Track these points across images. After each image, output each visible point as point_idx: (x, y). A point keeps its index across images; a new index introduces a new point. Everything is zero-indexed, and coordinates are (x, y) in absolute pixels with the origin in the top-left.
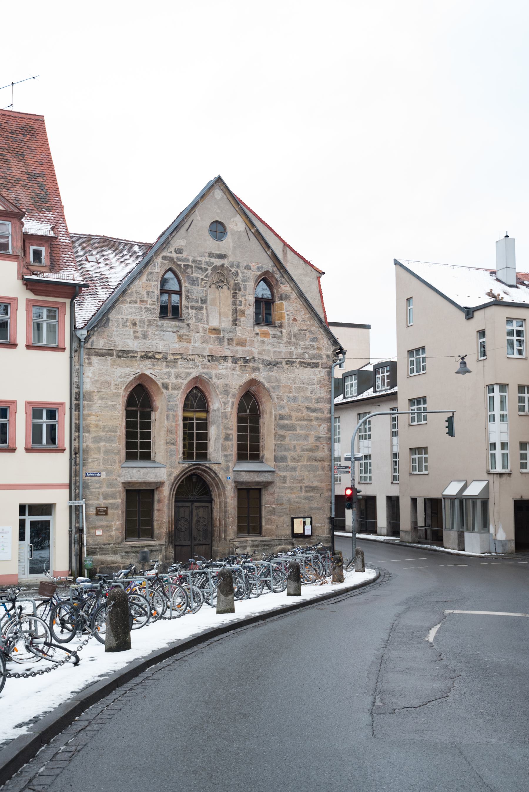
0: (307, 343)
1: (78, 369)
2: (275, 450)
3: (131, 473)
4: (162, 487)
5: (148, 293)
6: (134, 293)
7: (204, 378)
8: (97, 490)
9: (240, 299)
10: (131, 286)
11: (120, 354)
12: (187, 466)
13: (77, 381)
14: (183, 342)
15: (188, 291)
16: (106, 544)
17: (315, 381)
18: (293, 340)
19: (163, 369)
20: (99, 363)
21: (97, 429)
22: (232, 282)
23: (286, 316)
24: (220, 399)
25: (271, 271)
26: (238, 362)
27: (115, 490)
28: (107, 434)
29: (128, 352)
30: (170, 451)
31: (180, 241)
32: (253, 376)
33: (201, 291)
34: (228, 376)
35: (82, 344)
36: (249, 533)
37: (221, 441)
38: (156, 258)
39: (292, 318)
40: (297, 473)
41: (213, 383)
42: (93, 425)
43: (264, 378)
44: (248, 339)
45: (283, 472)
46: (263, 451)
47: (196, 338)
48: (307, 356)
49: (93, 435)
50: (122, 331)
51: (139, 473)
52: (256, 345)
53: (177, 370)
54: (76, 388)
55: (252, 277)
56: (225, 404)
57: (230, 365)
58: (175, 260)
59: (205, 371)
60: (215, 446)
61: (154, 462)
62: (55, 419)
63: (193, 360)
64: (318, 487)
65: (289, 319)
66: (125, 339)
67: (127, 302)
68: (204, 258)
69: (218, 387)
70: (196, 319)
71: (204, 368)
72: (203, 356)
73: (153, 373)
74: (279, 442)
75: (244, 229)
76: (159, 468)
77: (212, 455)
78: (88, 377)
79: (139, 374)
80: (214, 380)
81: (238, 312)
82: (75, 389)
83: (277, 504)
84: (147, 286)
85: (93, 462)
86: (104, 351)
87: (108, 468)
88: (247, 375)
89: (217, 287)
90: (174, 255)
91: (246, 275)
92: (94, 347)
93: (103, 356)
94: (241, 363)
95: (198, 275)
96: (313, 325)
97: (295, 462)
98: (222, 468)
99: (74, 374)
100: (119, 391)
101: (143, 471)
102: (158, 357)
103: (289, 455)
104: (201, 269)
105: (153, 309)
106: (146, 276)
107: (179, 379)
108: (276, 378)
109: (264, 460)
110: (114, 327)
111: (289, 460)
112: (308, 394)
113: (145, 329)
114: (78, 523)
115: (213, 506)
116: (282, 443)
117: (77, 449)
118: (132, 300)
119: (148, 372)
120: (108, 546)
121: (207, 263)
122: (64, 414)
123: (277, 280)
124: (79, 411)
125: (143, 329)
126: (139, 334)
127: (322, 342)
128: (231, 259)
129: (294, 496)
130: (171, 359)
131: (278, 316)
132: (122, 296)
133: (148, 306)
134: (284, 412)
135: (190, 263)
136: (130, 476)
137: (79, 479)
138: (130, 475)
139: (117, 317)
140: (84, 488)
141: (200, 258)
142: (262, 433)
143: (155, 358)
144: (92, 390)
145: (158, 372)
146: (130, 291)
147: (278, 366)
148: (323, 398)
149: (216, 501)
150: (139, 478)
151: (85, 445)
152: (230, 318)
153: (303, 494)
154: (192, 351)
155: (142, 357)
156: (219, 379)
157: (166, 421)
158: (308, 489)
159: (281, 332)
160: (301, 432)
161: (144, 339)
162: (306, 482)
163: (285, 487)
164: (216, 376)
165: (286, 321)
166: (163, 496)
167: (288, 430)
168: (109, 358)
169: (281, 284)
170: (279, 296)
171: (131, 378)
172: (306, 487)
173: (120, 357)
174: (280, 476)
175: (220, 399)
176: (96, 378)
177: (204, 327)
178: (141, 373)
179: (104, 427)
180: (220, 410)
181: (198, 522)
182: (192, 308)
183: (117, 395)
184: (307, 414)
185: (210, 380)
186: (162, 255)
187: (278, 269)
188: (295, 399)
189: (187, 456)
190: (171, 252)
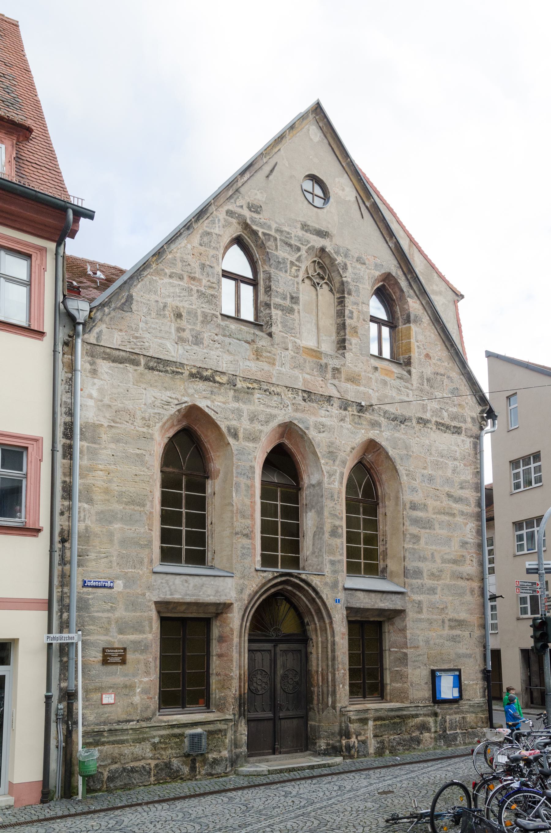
3: (171, 583)
4: (226, 613)
6: (178, 260)
7: (298, 429)
8: (106, 615)
9: (350, 308)
11: (151, 364)
12: (270, 576)
16: (122, 722)
17: (458, 454)
18: (426, 387)
21: (107, 497)
24: (323, 466)
25: (394, 274)
27: (141, 616)
28: (127, 507)
29: (167, 363)
30: (242, 548)
31: (256, 191)
32: (373, 434)
33: (291, 282)
34: (334, 428)
39: (425, 352)
40: (437, 596)
41: (310, 437)
42: (100, 488)
43: (387, 439)
45: (418, 594)
46: (384, 561)
48: (445, 414)
49: (99, 507)
50: (157, 323)
51: (186, 585)
53: (252, 408)
55: (367, 278)
58: (249, 221)
59: (298, 415)
60: (313, 545)
61: (212, 567)
65: (420, 354)
67: (166, 274)
68: (294, 230)
71: (296, 410)
73: (212, 407)
74: (411, 546)
75: (354, 199)
76: (222, 578)
77: (309, 562)
79: (186, 404)
80: (312, 434)
85: (96, 560)
86: (122, 353)
87: (127, 573)
88: (363, 431)
90: (247, 213)
91: (358, 272)
94: (353, 410)
95: (286, 255)
98: (326, 584)
102: (221, 381)
104: (290, 245)
105: (212, 295)
106: (199, 236)
107: (257, 423)
108: (404, 442)
109: (388, 575)
111: (425, 575)
112: (449, 473)
113: (198, 327)
114: (66, 679)
117: (66, 532)
118: (173, 273)
119: (202, 404)
122: (41, 460)
124: (71, 459)
126: (187, 335)
129: (434, 634)
131: (404, 348)
132: (156, 260)
133: (202, 289)
135: (272, 233)
136: (170, 590)
138: (169, 587)
139: (147, 296)
140: (79, 609)
142: (381, 532)
143: (215, 382)
145: (220, 407)
146: (170, 256)
147: (406, 424)
148: (469, 483)
149: (314, 640)
150: (187, 594)
151: (82, 526)
155: (192, 375)
156: (320, 432)
158: (453, 624)
159: (409, 372)
161: (196, 344)
162: (449, 613)
163: (420, 620)
164: (316, 426)
166: (228, 628)
167: (423, 528)
168: (130, 368)
170: (405, 316)
171: (173, 410)
172: (449, 620)
173: (152, 369)
176: (106, 401)
178: (190, 404)
179: (121, 494)
184: (448, 504)
185: (307, 431)
186: (226, 208)
187: (405, 274)
188: (431, 479)
190: (242, 207)
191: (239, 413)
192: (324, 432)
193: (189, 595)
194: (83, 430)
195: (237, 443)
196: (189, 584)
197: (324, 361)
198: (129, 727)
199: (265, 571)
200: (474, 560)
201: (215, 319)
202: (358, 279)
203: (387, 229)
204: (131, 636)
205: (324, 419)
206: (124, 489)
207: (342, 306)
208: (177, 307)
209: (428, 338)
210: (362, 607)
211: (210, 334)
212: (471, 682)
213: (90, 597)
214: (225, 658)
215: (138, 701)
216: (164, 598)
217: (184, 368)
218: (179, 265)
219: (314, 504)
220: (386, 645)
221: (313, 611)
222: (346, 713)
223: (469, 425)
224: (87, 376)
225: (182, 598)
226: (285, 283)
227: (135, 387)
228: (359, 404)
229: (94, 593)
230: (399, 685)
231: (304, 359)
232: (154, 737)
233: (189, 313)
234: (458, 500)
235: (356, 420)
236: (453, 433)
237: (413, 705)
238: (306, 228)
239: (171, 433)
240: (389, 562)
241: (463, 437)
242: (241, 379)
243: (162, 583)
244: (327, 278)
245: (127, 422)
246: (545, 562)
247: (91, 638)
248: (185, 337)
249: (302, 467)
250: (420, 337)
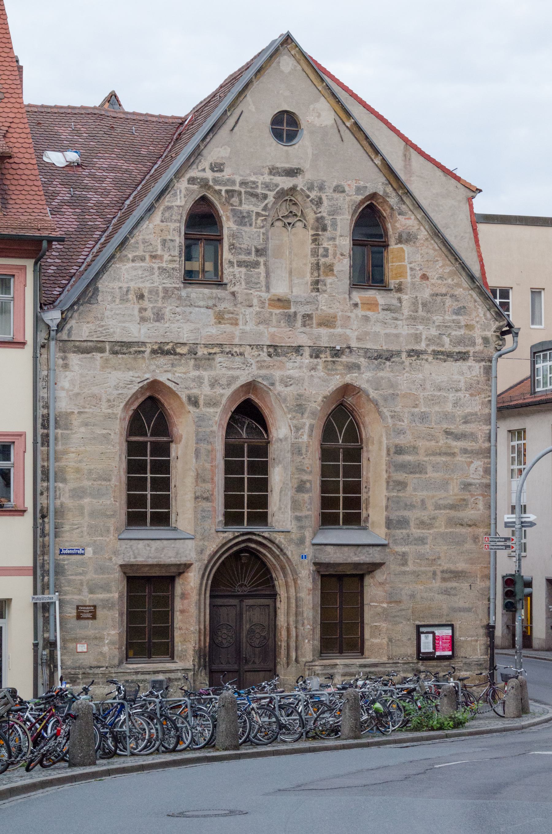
0: (447, 317)
1: (47, 376)
2: (387, 507)
3: (134, 548)
4: (188, 572)
5: (164, 242)
6: (140, 243)
7: (262, 386)
9: (325, 245)
10: (135, 232)
11: (117, 348)
12: (231, 536)
13: (46, 395)
14: (225, 324)
16: (94, 668)
18: (421, 313)
19: (189, 372)
20: (80, 365)
21: (79, 476)
22: (311, 217)
23: (408, 271)
26: (321, 356)
28: (95, 483)
31: (219, 149)
32: (349, 378)
34: (303, 380)
36: (341, 652)
38: (178, 181)
39: (420, 274)
40: (427, 546)
42: (72, 468)
43: (368, 381)
44: (340, 314)
45: (402, 545)
46: (367, 510)
47: (248, 317)
49: (71, 485)
50: (120, 308)
51: (148, 548)
52: (355, 324)
53: (213, 373)
54: (43, 407)
57: (307, 361)
58: (211, 183)
59: (263, 372)
60: (280, 501)
62: (10, 461)
63: (242, 354)
64: (466, 572)
65: (413, 276)
66: (124, 322)
67: (129, 259)
72: (259, 347)
73: (173, 380)
74: (395, 494)
75: (333, 122)
76: (182, 541)
78: (63, 389)
79: (148, 381)
81: (322, 268)
82: (42, 409)
84: (162, 231)
86: (89, 344)
87: (95, 541)
88: (338, 377)
90: (209, 175)
92: (73, 338)
93: (88, 353)
94: (326, 357)
96: (458, 285)
97: (424, 529)
99: (40, 384)
100: (115, 412)
102: (181, 352)
103: (412, 515)
107: (218, 387)
108: (389, 381)
110: (106, 303)
112: (449, 407)
113: (160, 304)
116: (401, 494)
117: (45, 509)
119: (163, 378)
120: (97, 671)
121: (267, 186)
125: (155, 305)
128: (309, 176)
129: (422, 587)
130: (204, 354)
133: (164, 265)
135: (237, 188)
136: (134, 554)
137: (49, 560)
138: (133, 552)
139: (111, 285)
140: (57, 573)
141: (254, 177)
143: (175, 354)
144: (69, 411)
147: (393, 360)
148: (477, 415)
150: (148, 557)
151: (58, 502)
152: (309, 278)
153: (438, 585)
154: (240, 339)
155: (154, 352)
156: (286, 386)
157: (194, 460)
158: (446, 576)
159: (400, 300)
160: (435, 475)
161: (158, 321)
162: (443, 564)
163: (404, 573)
164: (282, 381)
168: (98, 355)
169: (399, 214)
170: (397, 235)
171: (135, 388)
172: (443, 572)
173: (115, 353)
174: (396, 552)
175: (289, 421)
176: (76, 390)
177: (260, 297)
178: (151, 379)
179: (90, 472)
180: (289, 440)
181: (251, 631)
185: (272, 388)
186: (188, 176)
187: (394, 189)
188: (424, 417)
190: (204, 170)
192: (291, 385)
193: (151, 557)
194: (58, 419)
195: (197, 411)
196: (151, 548)
198: (99, 672)
199: (226, 532)
203: (372, 147)
204: (100, 595)
205: (291, 371)
206: (92, 467)
207: (316, 245)
208: (139, 288)
209: (426, 256)
210: (332, 562)
211: (171, 308)
212: (469, 639)
213: (65, 563)
214: (187, 614)
215: (107, 651)
216: (128, 561)
217: (145, 346)
218: (141, 247)
219: (281, 459)
222: (311, 667)
224: (60, 371)
225: (144, 561)
226: (250, 238)
227: (101, 372)
229: (68, 560)
231: (270, 312)
234: (461, 437)
236: (456, 360)
237: (391, 661)
238: (275, 171)
242: (202, 346)
243: (126, 548)
244: (299, 214)
245: (95, 406)
248: (147, 316)
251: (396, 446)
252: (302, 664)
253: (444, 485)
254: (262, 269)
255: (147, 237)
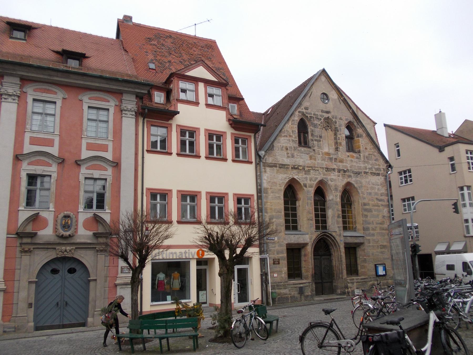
0: (373, 162)
1: (259, 175)
5: (293, 131)
9: (338, 136)
11: (281, 166)
13: (259, 182)
15: (312, 131)
18: (366, 160)
22: (333, 127)
25: (352, 121)
26: (341, 172)
29: (284, 165)
31: (306, 103)
32: (349, 180)
35: (262, 159)
36: (351, 275)
37: (336, 218)
39: (365, 147)
40: (375, 237)
41: (329, 184)
43: (354, 181)
49: (269, 214)
52: (349, 162)
53: (310, 176)
55: (343, 124)
56: (336, 196)
58: (305, 113)
59: (325, 177)
60: (332, 221)
61: (300, 231)
63: (318, 170)
66: (282, 157)
69: (332, 186)
70: (318, 147)
71: (324, 175)
72: (323, 168)
77: (331, 227)
78: (265, 179)
81: (338, 143)
83: (367, 256)
86: (272, 164)
88: (346, 179)
89: (326, 130)
90: (304, 111)
92: (267, 162)
93: (272, 167)
94: (342, 172)
95: (317, 122)
96: (375, 152)
98: (337, 235)
99: (258, 177)
101: (297, 236)
102: (300, 168)
103: (370, 226)
104: (318, 119)
105: (296, 140)
108: (360, 181)
109: (357, 230)
112: (376, 191)
114: (265, 269)
115: (332, 258)
116: (367, 219)
119: (295, 177)
121: (321, 116)
123: (355, 126)
126: (290, 155)
127: (380, 161)
133: (293, 139)
134: (366, 201)
135: (312, 116)
136: (290, 240)
143: (299, 169)
144: (267, 187)
147: (360, 174)
149: (334, 255)
152: (334, 147)
154: (317, 165)
155: (292, 168)
156: (332, 182)
158: (382, 247)
159: (360, 155)
160: (375, 213)
163: (370, 246)
165: (361, 149)
167: (369, 212)
168: (275, 168)
171: (287, 180)
172: (380, 246)
173: (280, 168)
176: (269, 180)
179: (275, 209)
182: (316, 140)
183: (280, 190)
185: (327, 182)
186: (298, 110)
188: (370, 194)
189: (317, 228)
190: (302, 109)
191: (306, 178)
197: (331, 156)
200: (388, 222)
201: (297, 148)
202: (340, 126)
206: (275, 208)
218: (286, 132)
220: (358, 255)
221: (333, 244)
223: (382, 172)
228: (344, 170)
230: (364, 270)
232: (289, 288)
233: (290, 148)
234: (380, 200)
235: (343, 176)
237: (369, 277)
239: (286, 187)
240: (357, 225)
241: (380, 177)
244: (330, 126)
246: (414, 224)
247: (270, 256)
249: (326, 193)
250: (363, 142)
251: (364, 203)
252: (344, 279)
253: (378, 216)
254: (321, 143)
255: (287, 129)
